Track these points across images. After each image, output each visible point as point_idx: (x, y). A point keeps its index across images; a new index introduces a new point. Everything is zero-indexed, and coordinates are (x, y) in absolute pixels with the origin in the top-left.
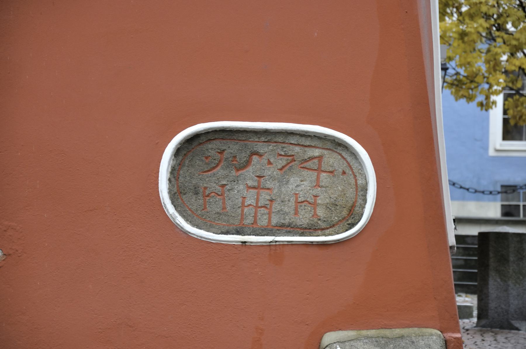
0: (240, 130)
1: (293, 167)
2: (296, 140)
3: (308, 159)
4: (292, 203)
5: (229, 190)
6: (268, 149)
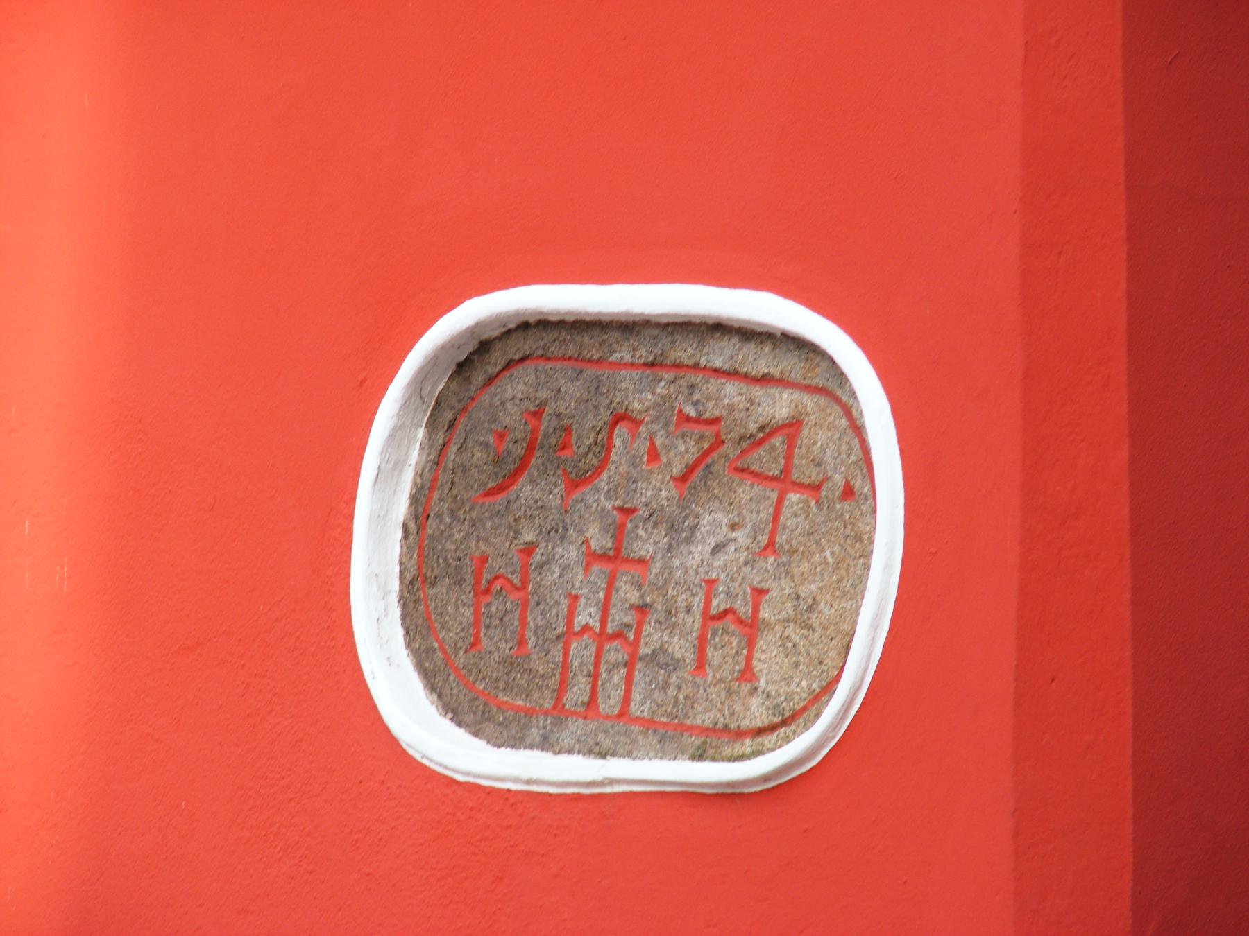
0: (705, 324)
1: (714, 468)
2: (728, 353)
3: (761, 435)
4: (694, 622)
5: (541, 566)
6: (653, 394)
